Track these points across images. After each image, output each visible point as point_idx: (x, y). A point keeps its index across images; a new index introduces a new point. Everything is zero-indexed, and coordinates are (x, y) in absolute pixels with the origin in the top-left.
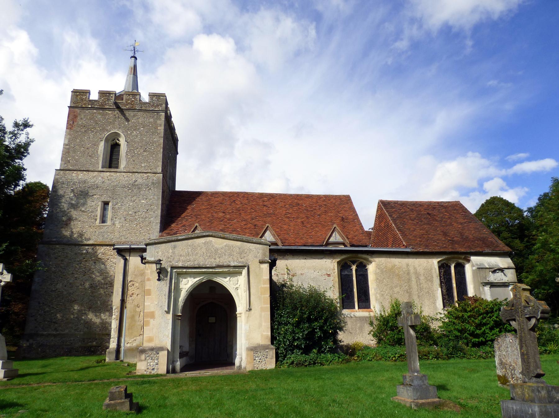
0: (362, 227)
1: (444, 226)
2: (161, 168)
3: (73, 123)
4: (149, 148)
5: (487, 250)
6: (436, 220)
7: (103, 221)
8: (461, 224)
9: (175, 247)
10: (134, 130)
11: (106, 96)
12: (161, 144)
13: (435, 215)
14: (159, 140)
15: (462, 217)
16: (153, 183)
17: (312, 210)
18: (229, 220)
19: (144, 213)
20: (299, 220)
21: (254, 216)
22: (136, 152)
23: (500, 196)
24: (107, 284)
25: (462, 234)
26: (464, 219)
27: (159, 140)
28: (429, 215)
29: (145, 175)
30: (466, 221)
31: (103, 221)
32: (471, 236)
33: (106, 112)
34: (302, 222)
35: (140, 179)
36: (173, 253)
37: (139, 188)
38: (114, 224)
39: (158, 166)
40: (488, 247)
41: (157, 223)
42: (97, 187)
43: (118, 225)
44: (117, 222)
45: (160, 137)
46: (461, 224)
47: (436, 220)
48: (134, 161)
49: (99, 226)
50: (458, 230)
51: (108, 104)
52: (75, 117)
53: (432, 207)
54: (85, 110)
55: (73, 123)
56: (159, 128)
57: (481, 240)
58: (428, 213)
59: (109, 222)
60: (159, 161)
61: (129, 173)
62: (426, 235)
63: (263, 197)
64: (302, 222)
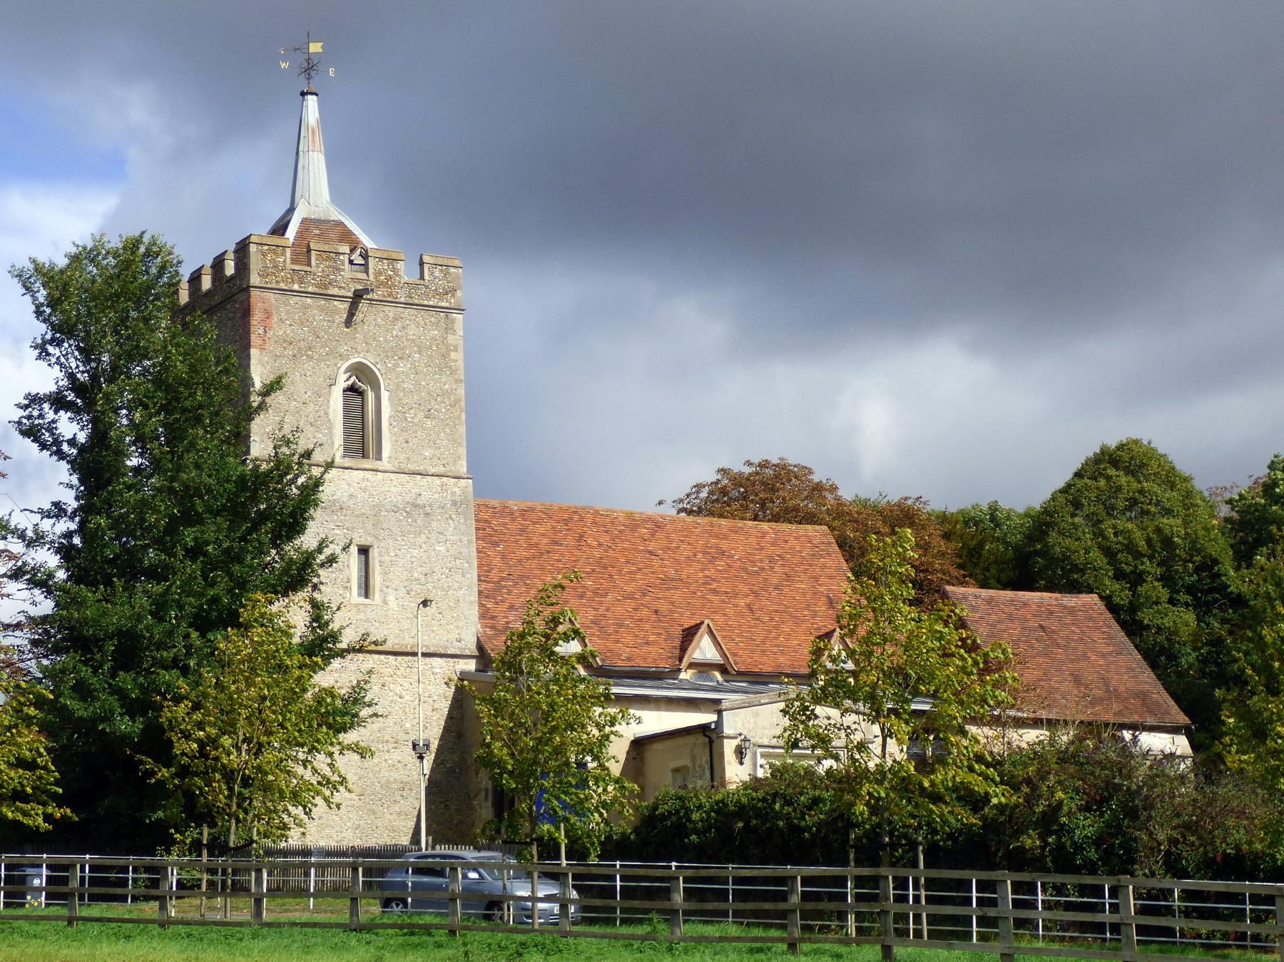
0: (249, 280)
1: (1074, 660)
2: (465, 463)
3: (265, 332)
4: (435, 410)
5: (1150, 721)
6: (1058, 646)
7: (366, 590)
8: (1103, 656)
9: (757, 714)
10: (400, 358)
11: (329, 259)
12: (460, 400)
13: (1054, 632)
14: (456, 390)
15: (1103, 639)
16: (454, 503)
17: (756, 572)
18: (595, 593)
19: (444, 577)
20: (742, 603)
21: (643, 584)
22: (409, 419)
23: (1149, 443)
24: (387, 742)
25: (1106, 682)
26: (1108, 645)
27: (456, 390)
28: (1044, 631)
29: (437, 481)
30: (1111, 648)
31: (366, 590)
32: (1122, 688)
33: (334, 306)
34: (749, 606)
35: (428, 490)
36: (756, 723)
37: (427, 514)
38: (385, 602)
39: (459, 458)
40: (1150, 712)
41: (472, 602)
42: (341, 508)
43: (393, 603)
44: (391, 598)
45: (457, 381)
46: (1103, 656)
47: (1058, 646)
48: (407, 442)
49: (357, 605)
50: (1098, 672)
51: (336, 281)
52: (267, 315)
53: (1047, 609)
54: (288, 297)
55: (265, 332)
56: (453, 355)
57: (1138, 697)
58: (1040, 626)
59: (377, 596)
60: (460, 444)
61: (402, 475)
62: (1045, 680)
63: (638, 526)
64: (749, 606)
